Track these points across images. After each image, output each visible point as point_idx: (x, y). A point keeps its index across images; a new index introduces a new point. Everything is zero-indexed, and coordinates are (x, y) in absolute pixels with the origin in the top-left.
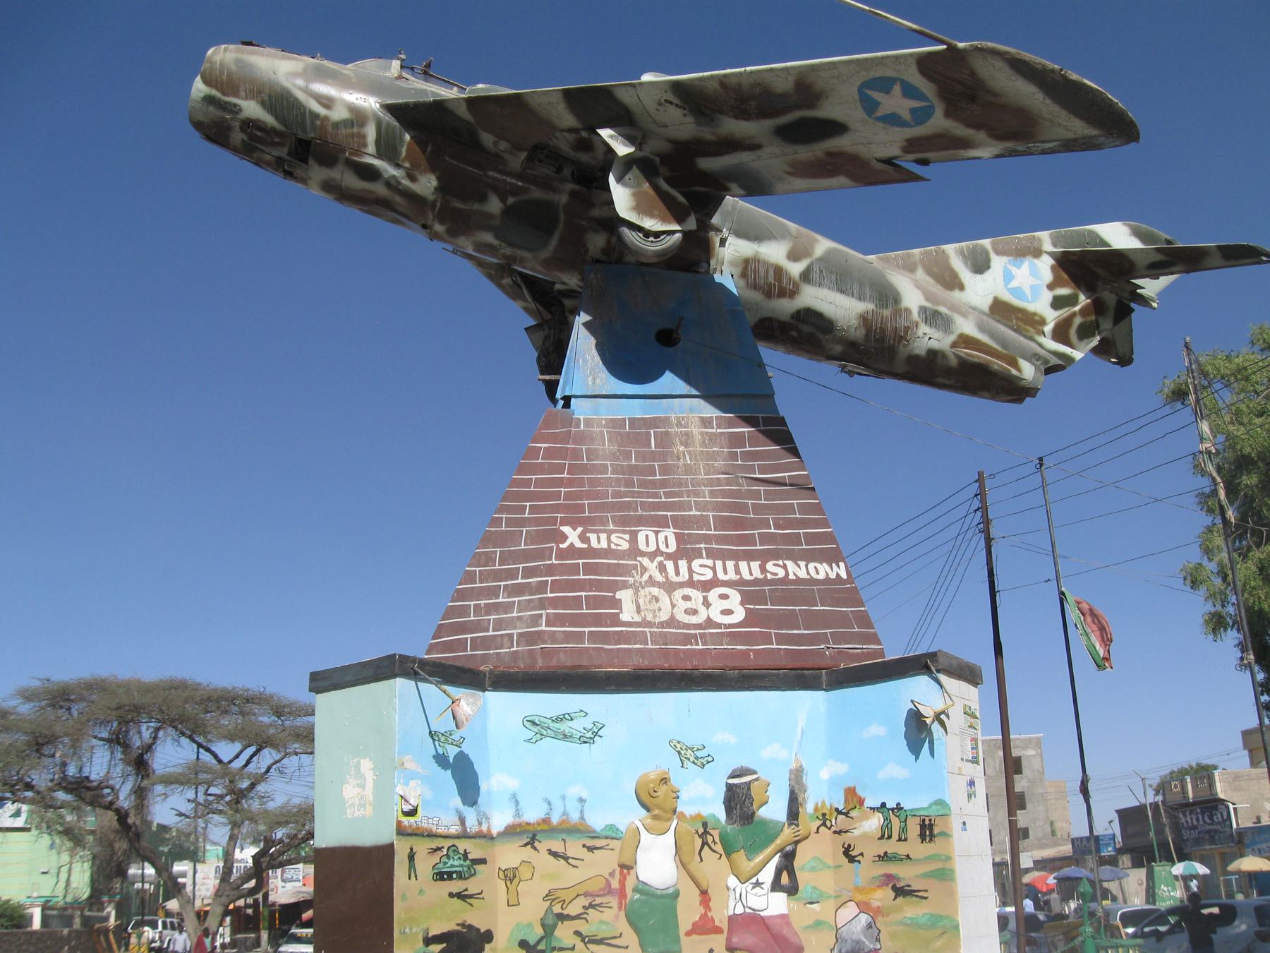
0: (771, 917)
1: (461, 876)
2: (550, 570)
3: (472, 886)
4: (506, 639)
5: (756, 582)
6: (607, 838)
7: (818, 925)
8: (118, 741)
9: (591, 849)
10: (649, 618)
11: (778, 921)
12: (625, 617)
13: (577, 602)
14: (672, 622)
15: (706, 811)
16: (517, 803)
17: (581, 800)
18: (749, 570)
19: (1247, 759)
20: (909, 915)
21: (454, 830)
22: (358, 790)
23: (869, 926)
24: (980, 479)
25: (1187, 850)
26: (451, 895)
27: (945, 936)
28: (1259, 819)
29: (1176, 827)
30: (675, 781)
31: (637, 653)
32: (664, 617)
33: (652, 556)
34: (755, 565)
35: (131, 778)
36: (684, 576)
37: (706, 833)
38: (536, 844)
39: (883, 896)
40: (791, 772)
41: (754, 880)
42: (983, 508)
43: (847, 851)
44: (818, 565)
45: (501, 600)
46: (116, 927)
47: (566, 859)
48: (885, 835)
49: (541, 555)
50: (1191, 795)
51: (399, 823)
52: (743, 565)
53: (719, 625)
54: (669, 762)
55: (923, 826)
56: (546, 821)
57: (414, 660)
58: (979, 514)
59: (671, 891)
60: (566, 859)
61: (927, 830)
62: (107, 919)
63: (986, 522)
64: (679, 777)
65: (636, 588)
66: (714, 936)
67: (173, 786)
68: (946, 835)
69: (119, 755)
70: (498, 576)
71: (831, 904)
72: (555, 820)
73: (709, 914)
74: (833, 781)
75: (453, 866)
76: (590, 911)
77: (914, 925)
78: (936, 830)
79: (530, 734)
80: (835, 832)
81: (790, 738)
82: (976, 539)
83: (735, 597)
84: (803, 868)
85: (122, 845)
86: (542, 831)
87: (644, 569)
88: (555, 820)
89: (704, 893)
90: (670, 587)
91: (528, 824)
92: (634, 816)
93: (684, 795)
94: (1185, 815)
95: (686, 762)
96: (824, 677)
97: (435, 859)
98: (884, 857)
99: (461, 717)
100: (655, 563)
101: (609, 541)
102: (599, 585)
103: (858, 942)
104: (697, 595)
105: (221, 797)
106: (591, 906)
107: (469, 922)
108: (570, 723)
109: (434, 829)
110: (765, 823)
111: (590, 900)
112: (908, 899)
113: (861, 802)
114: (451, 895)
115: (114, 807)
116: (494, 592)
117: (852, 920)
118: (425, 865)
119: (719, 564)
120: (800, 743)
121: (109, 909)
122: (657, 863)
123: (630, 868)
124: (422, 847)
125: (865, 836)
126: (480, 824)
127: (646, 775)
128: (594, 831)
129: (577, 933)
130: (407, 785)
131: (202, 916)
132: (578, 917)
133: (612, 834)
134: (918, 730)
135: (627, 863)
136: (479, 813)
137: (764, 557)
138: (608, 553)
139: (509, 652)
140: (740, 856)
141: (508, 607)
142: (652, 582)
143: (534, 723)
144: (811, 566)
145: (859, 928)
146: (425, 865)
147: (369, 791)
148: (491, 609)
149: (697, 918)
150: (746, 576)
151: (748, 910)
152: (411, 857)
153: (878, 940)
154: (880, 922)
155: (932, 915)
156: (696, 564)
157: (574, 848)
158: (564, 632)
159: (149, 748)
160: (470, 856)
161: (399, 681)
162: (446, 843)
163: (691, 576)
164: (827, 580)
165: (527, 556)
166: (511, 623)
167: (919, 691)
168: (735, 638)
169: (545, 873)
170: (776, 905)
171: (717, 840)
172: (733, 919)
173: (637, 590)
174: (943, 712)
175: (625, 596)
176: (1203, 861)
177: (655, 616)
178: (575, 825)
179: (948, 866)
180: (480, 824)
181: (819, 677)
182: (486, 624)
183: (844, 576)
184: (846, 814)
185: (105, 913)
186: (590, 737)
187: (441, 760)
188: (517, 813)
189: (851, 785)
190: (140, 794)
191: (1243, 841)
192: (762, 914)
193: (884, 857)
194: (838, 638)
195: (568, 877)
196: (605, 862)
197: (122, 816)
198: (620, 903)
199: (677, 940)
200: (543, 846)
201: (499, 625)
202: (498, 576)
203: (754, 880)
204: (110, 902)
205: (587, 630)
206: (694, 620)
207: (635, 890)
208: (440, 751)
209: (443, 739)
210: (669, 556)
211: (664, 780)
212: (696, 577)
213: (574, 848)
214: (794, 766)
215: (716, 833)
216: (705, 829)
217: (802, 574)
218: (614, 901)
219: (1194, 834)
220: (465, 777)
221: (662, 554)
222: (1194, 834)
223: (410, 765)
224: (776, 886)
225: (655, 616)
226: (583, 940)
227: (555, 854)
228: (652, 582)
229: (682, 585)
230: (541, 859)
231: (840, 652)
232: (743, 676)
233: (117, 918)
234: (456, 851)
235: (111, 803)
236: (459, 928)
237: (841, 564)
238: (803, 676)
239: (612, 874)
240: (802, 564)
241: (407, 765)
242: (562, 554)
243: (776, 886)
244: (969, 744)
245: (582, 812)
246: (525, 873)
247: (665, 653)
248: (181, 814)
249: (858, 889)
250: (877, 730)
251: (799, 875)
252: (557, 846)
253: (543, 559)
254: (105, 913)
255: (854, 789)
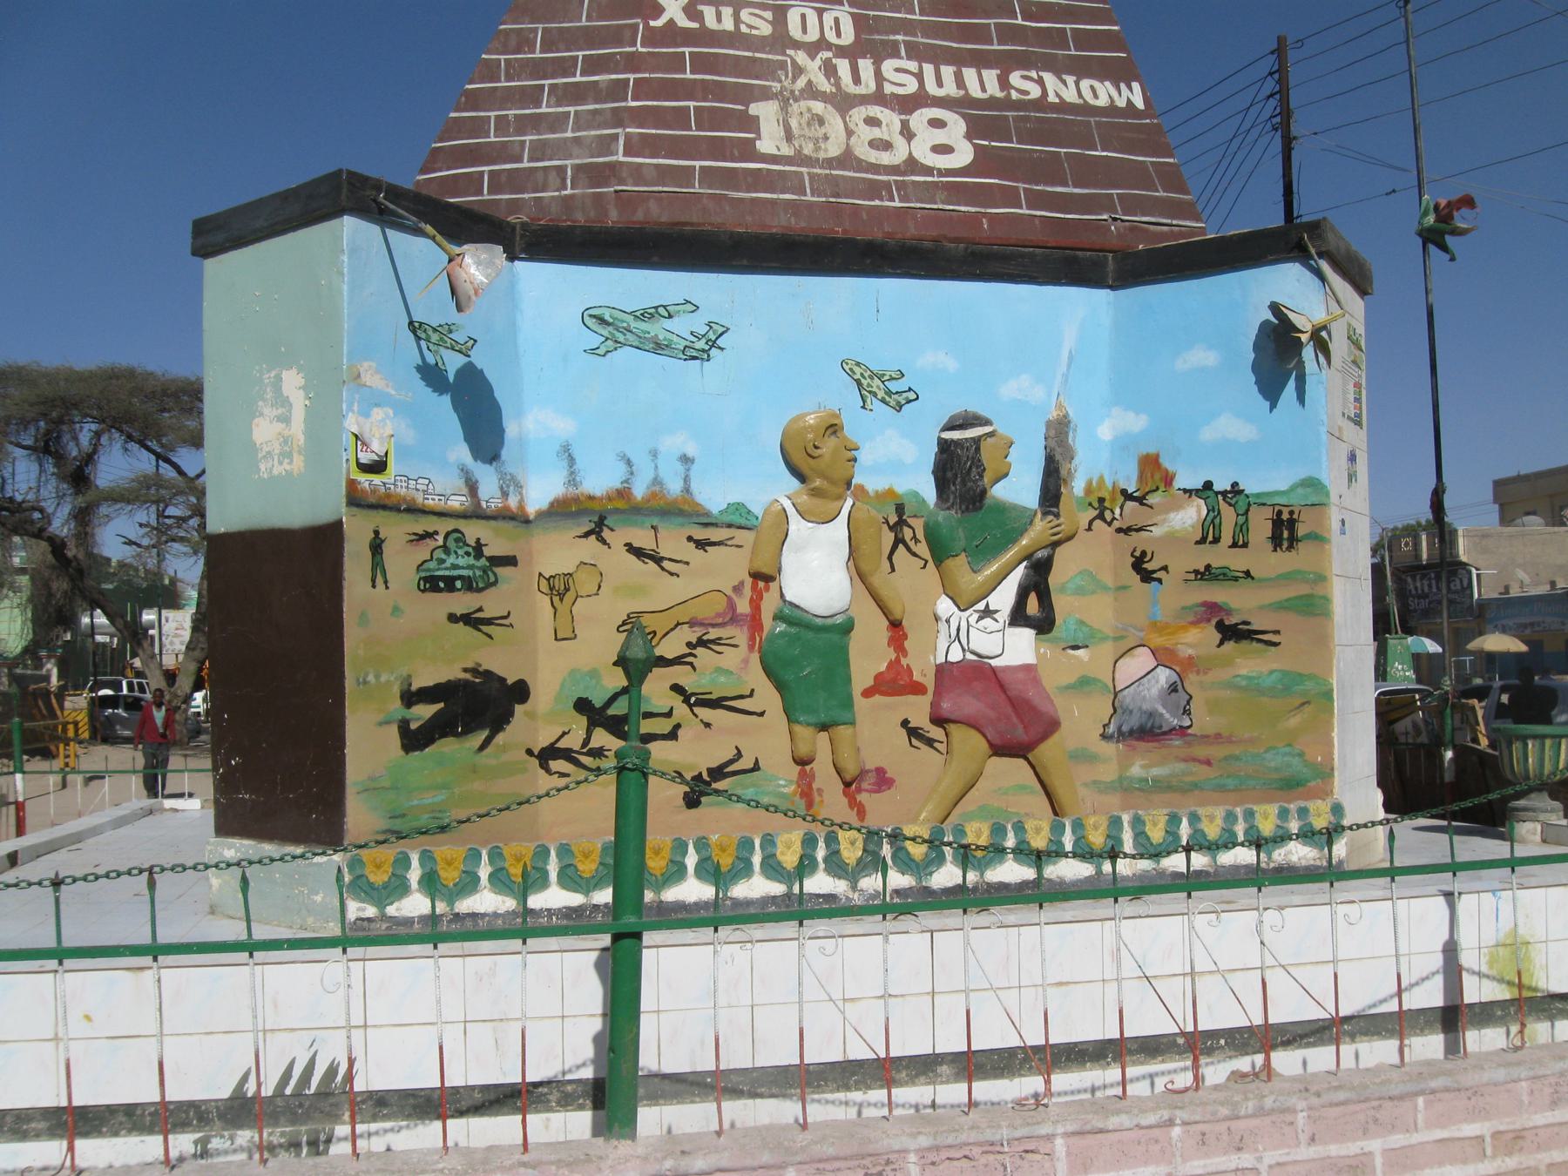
0: (1007, 668)
1: (469, 584)
2: (633, 62)
3: (490, 603)
4: (553, 175)
5: (991, 103)
6: (730, 526)
7: (1084, 684)
8: (47, 448)
9: (702, 545)
10: (808, 150)
11: (1021, 675)
12: (765, 146)
13: (681, 117)
14: (847, 159)
15: (902, 486)
16: (571, 460)
17: (686, 460)
18: (982, 83)
19: (1496, 517)
20: (1244, 672)
21: (457, 503)
22: (280, 426)
23: (1173, 689)
24: (1280, 51)
25: (1412, 623)
26: (452, 618)
27: (1307, 708)
28: (1507, 589)
29: (1402, 595)
30: (849, 431)
31: (781, 209)
32: (833, 150)
33: (813, 49)
34: (991, 76)
35: (68, 499)
36: (869, 85)
37: (901, 522)
38: (606, 534)
39: (1199, 640)
40: (1049, 424)
41: (981, 606)
42: (1282, 93)
43: (1139, 564)
44: (1097, 84)
45: (544, 110)
46: (60, 688)
47: (658, 560)
48: (1209, 535)
49: (616, 37)
50: (1425, 556)
51: (352, 484)
52: (970, 74)
53: (929, 171)
54: (842, 398)
55: (1278, 523)
56: (623, 493)
57: (377, 185)
58: (1273, 102)
59: (839, 620)
60: (658, 560)
61: (1285, 531)
62: (47, 678)
63: (1286, 113)
64: (856, 425)
65: (785, 100)
66: (911, 698)
67: (118, 506)
68: (1318, 538)
69: (51, 469)
70: (539, 69)
71: (1107, 650)
72: (639, 491)
73: (904, 662)
74: (1121, 444)
75: (455, 567)
76: (700, 651)
77: (1252, 688)
78: (1301, 530)
79: (595, 340)
80: (1119, 530)
81: (1046, 366)
82: (1265, 139)
83: (956, 127)
84: (1063, 589)
85: (61, 585)
86: (617, 511)
87: (799, 71)
88: (639, 491)
89: (895, 625)
90: (843, 103)
91: (591, 498)
92: (781, 489)
93: (864, 457)
94: (1414, 580)
95: (869, 398)
96: (1111, 266)
97: (422, 552)
98: (1206, 574)
99: (465, 288)
100: (818, 61)
101: (737, 20)
102: (720, 91)
103: (1151, 714)
104: (891, 119)
105: (184, 519)
106: (702, 643)
107: (485, 667)
108: (667, 324)
109: (419, 498)
110: (1003, 509)
111: (699, 631)
112: (1245, 644)
113: (1168, 480)
114: (452, 618)
115: (46, 535)
116: (533, 96)
117: (1142, 677)
118: (403, 563)
119: (928, 69)
120: (1066, 377)
121: (49, 666)
122: (816, 573)
123: (768, 579)
124: (396, 531)
125: (1172, 539)
126: (505, 494)
127: (802, 417)
128: (708, 514)
129: (677, 688)
130: (367, 415)
131: (171, 676)
132: (678, 661)
133: (738, 520)
134: (1280, 351)
135: (766, 570)
136: (502, 476)
137: (1004, 64)
138: (735, 38)
139: (559, 195)
140: (959, 565)
141: (558, 122)
142: (811, 92)
143: (602, 320)
144: (1085, 84)
145: (1155, 691)
146: (403, 563)
147: (297, 427)
148: (524, 124)
149: (883, 667)
150: (976, 92)
151: (970, 657)
152: (377, 547)
153: (1187, 712)
154: (1192, 682)
155: (1285, 673)
156: (888, 66)
157: (672, 542)
158: (657, 166)
159: (89, 458)
160: (487, 552)
161: (349, 223)
162: (444, 526)
163: (880, 86)
164: (1112, 110)
165: (590, 38)
166: (562, 149)
167: (1291, 287)
168: (957, 192)
169: (619, 587)
170: (1017, 648)
171: (920, 536)
172: (943, 670)
173: (785, 108)
174: (1324, 328)
175: (766, 112)
176: (1435, 636)
177: (817, 149)
178: (675, 501)
179: (1318, 591)
180: (505, 494)
181: (1099, 265)
182: (517, 148)
183: (1139, 103)
184: (1140, 500)
185: (44, 672)
186: (702, 349)
187: (432, 375)
188: (572, 480)
189: (1152, 450)
190: (83, 518)
191: (1484, 616)
192: (993, 662)
193: (1206, 574)
194: (1131, 205)
195: (659, 593)
196: (723, 570)
197: (57, 546)
198: (752, 639)
199: (848, 703)
200: (618, 537)
201: (539, 151)
202: (539, 69)
203: (981, 606)
204: (49, 657)
205: (697, 164)
206: (885, 158)
207: (779, 617)
208: (431, 359)
209: (435, 337)
210: (842, 52)
211: (833, 428)
212: (888, 89)
213: (672, 542)
214: (1053, 414)
215: (918, 524)
216: (900, 514)
217: (1070, 96)
218: (740, 635)
219: (1424, 604)
220: (478, 410)
221: (829, 46)
222: (1424, 604)
223: (371, 379)
224: (1018, 617)
225: (817, 149)
226: (686, 701)
227: (638, 553)
228: (811, 92)
229: (864, 100)
230: (615, 561)
231: (1134, 229)
232: (973, 253)
233: (60, 678)
234: (461, 540)
235: (42, 530)
236: (468, 676)
237: (1136, 86)
238: (1075, 258)
239: (738, 589)
240: (1070, 80)
241: (367, 378)
242: (653, 37)
243: (1018, 617)
244: (1351, 389)
245: (686, 479)
246: (585, 583)
247: (835, 210)
248: (130, 543)
249: (1157, 627)
250: (1203, 357)
251: (1060, 602)
252: (643, 539)
253: (620, 43)
254: (44, 672)
255: (1157, 456)
